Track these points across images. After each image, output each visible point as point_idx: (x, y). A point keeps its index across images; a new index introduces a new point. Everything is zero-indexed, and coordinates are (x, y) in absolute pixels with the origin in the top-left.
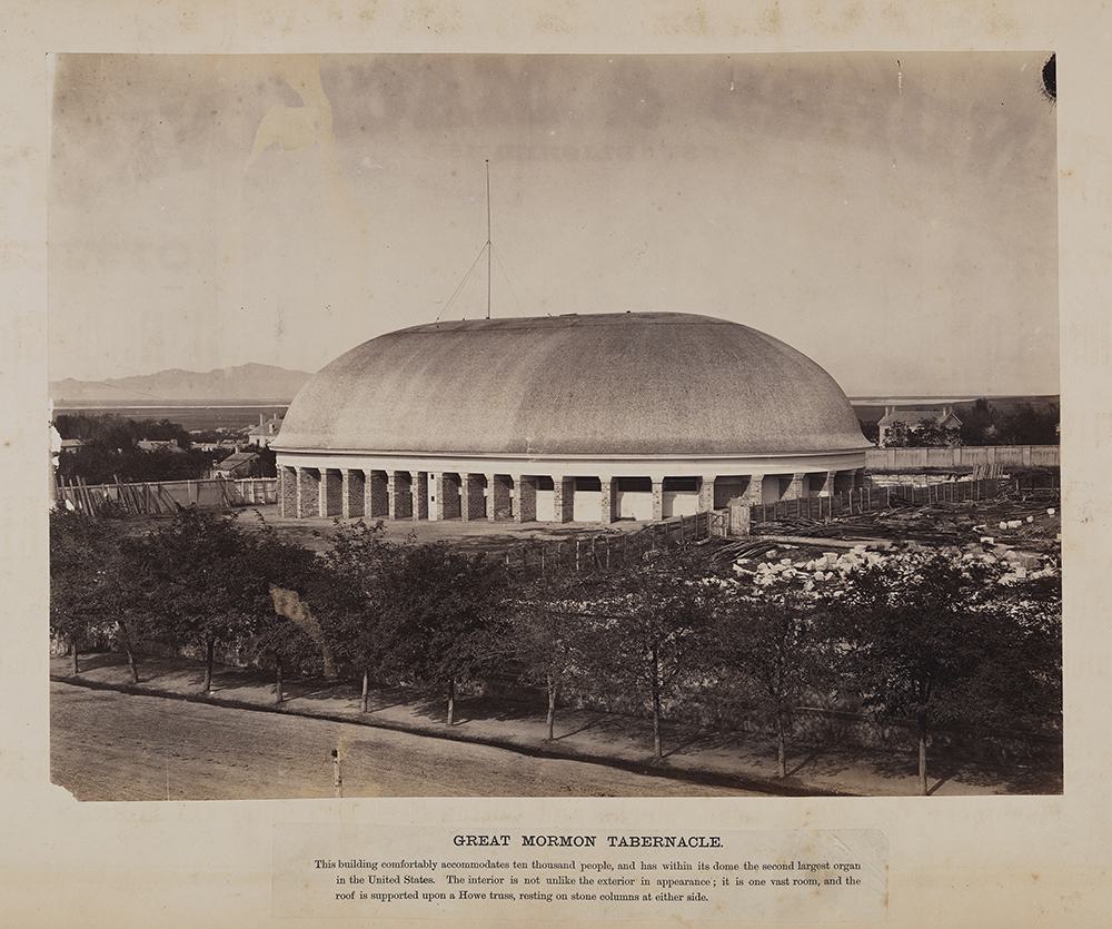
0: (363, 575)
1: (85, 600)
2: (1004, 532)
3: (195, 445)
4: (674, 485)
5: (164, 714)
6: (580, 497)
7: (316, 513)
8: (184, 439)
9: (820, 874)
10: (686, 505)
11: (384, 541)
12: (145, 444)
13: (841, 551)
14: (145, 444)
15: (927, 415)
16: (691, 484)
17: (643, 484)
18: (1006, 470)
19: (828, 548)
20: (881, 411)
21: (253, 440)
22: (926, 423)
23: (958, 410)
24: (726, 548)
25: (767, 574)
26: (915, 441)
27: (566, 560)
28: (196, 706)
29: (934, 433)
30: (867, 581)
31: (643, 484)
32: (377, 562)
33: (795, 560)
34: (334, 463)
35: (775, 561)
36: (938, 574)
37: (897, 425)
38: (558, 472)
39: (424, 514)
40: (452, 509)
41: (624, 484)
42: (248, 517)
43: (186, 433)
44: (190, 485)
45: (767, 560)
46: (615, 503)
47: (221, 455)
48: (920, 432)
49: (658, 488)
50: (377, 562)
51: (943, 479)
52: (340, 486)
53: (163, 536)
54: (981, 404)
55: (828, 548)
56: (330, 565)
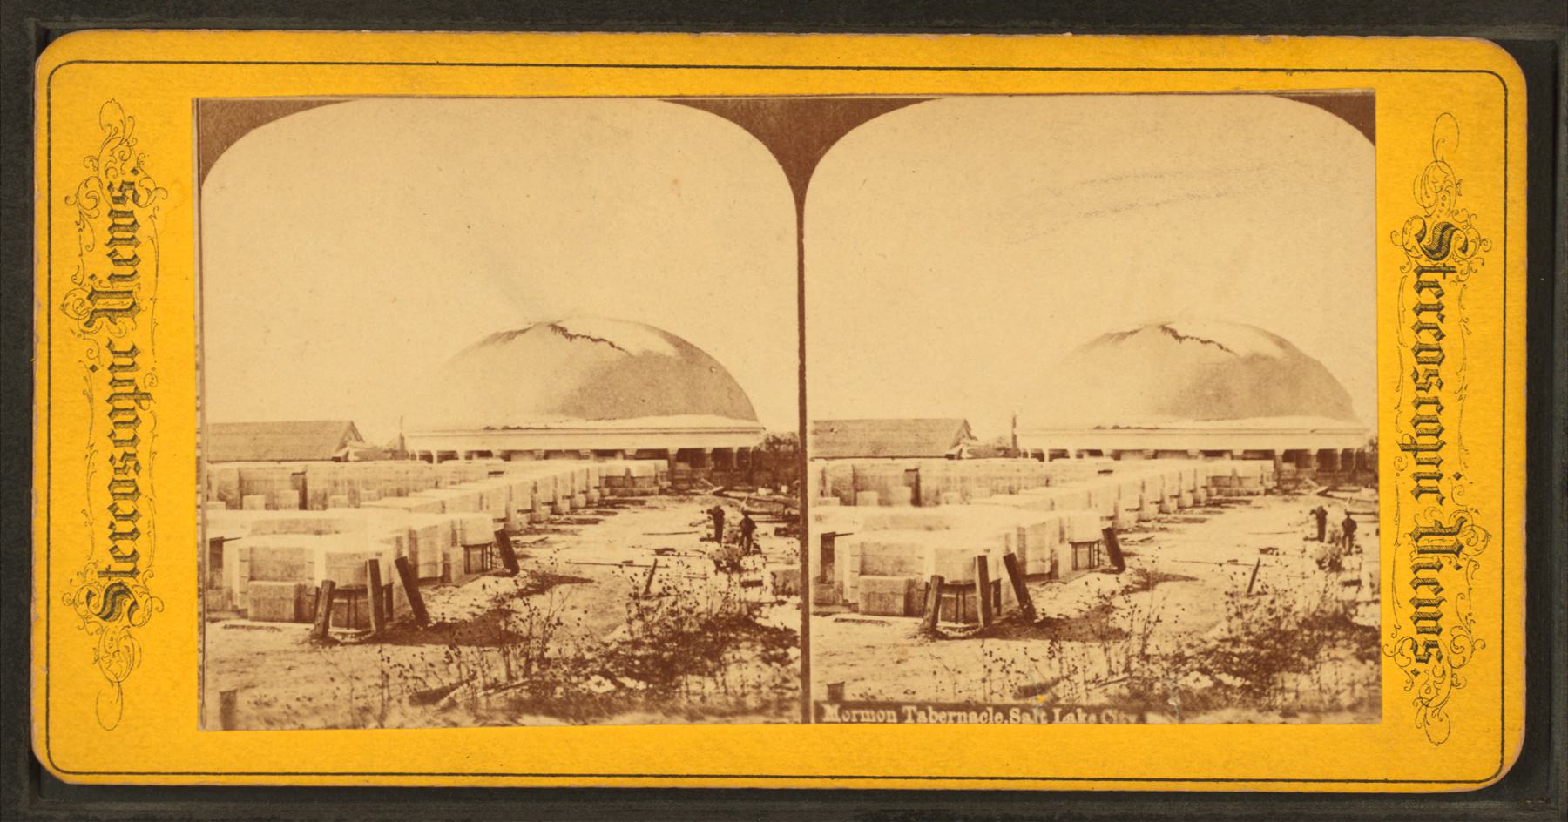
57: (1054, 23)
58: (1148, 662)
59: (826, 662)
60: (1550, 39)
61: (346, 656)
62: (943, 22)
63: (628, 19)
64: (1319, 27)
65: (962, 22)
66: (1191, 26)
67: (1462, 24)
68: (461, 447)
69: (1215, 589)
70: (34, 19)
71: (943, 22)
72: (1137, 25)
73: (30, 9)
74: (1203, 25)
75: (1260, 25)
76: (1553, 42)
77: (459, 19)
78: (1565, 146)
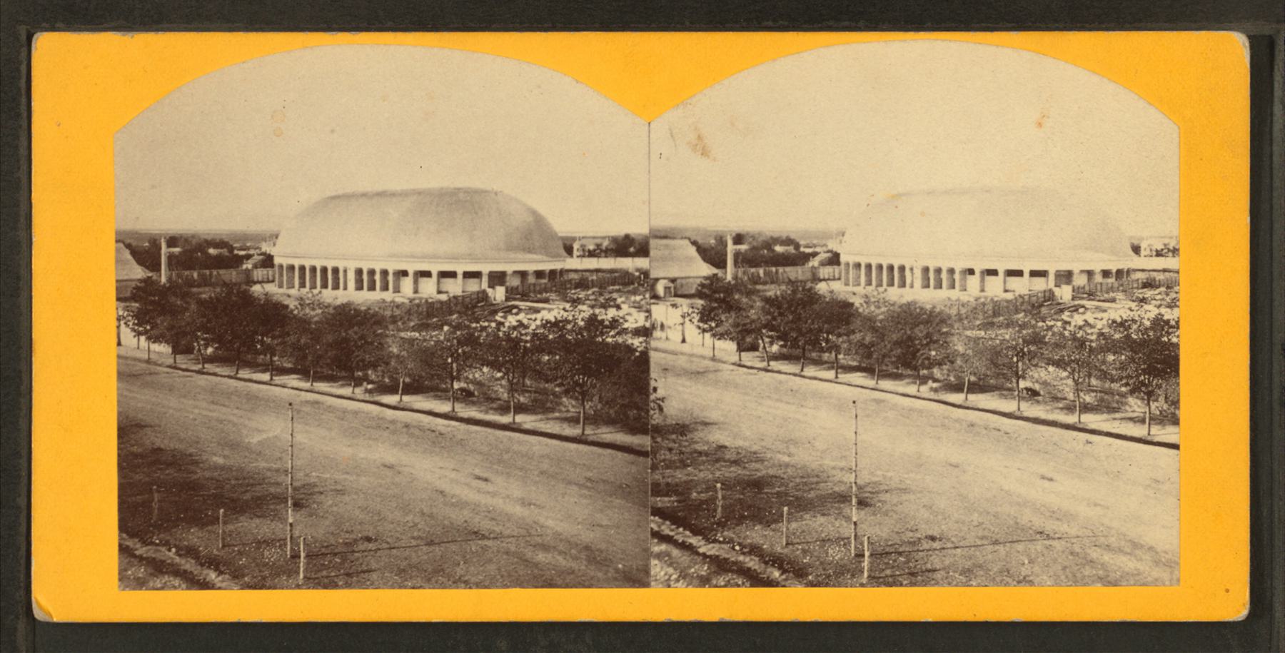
0: (312, 317)
1: (744, 325)
2: (634, 302)
3: (236, 252)
4: (468, 275)
5: (781, 382)
6: (989, 279)
7: (859, 285)
8: (231, 249)
9: (1089, 442)
10: (473, 286)
11: (322, 300)
12: (212, 251)
13: (550, 310)
14: (212, 251)
15: (598, 241)
16: (477, 275)
17: (452, 275)
18: (638, 270)
19: (544, 309)
20: (574, 239)
21: (263, 250)
22: (1165, 245)
23: (614, 240)
24: (492, 308)
25: (512, 320)
26: (592, 254)
27: (409, 312)
28: (232, 381)
29: (602, 251)
30: (556, 325)
31: (452, 275)
32: (319, 311)
33: (527, 314)
34: (290, 261)
35: (517, 314)
36: (593, 322)
37: (583, 246)
38: (412, 268)
39: (345, 288)
40: (359, 287)
41: (444, 275)
42: (257, 289)
43: (231, 246)
44: (799, 269)
45: (512, 314)
46: (439, 283)
47: (249, 257)
48: (595, 250)
49: (460, 276)
50: (883, 309)
51: (604, 275)
52: (294, 273)
53: (782, 294)
54: (627, 237)
55: (544, 309)
56: (296, 312)
57: (861, 23)
58: (671, 453)
59: (246, 460)
60: (1267, 33)
61: (166, 442)
62: (770, 23)
63: (512, 23)
64: (1078, 25)
65: (786, 23)
66: (973, 25)
67: (1195, 22)
68: (460, 269)
69: (399, 473)
70: (25, 27)
71: (770, 23)
72: (929, 24)
73: (21, 18)
74: (983, 25)
75: (1030, 24)
76: (1270, 37)
77: (374, 24)
78: (585, 450)
